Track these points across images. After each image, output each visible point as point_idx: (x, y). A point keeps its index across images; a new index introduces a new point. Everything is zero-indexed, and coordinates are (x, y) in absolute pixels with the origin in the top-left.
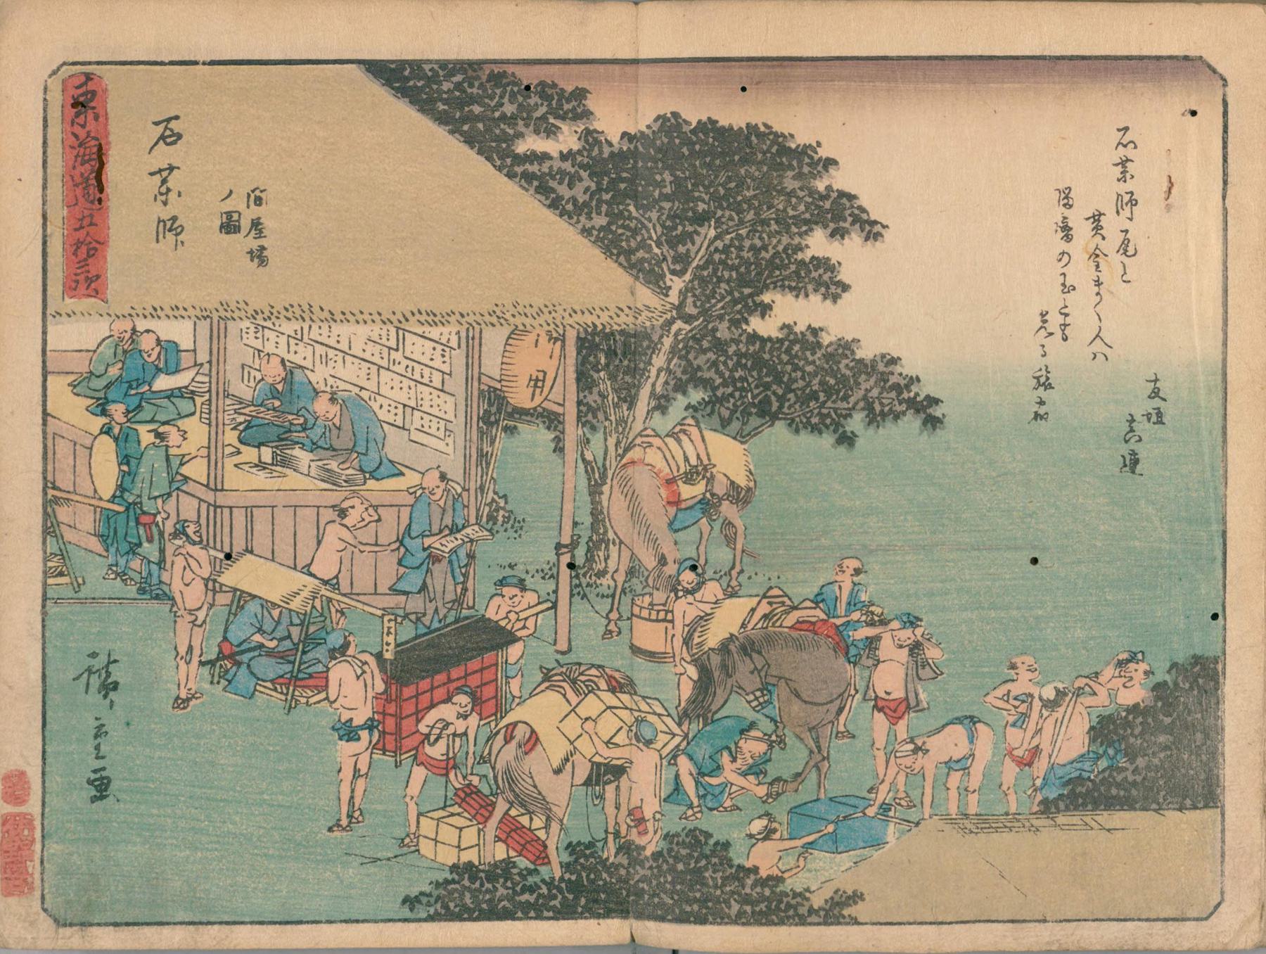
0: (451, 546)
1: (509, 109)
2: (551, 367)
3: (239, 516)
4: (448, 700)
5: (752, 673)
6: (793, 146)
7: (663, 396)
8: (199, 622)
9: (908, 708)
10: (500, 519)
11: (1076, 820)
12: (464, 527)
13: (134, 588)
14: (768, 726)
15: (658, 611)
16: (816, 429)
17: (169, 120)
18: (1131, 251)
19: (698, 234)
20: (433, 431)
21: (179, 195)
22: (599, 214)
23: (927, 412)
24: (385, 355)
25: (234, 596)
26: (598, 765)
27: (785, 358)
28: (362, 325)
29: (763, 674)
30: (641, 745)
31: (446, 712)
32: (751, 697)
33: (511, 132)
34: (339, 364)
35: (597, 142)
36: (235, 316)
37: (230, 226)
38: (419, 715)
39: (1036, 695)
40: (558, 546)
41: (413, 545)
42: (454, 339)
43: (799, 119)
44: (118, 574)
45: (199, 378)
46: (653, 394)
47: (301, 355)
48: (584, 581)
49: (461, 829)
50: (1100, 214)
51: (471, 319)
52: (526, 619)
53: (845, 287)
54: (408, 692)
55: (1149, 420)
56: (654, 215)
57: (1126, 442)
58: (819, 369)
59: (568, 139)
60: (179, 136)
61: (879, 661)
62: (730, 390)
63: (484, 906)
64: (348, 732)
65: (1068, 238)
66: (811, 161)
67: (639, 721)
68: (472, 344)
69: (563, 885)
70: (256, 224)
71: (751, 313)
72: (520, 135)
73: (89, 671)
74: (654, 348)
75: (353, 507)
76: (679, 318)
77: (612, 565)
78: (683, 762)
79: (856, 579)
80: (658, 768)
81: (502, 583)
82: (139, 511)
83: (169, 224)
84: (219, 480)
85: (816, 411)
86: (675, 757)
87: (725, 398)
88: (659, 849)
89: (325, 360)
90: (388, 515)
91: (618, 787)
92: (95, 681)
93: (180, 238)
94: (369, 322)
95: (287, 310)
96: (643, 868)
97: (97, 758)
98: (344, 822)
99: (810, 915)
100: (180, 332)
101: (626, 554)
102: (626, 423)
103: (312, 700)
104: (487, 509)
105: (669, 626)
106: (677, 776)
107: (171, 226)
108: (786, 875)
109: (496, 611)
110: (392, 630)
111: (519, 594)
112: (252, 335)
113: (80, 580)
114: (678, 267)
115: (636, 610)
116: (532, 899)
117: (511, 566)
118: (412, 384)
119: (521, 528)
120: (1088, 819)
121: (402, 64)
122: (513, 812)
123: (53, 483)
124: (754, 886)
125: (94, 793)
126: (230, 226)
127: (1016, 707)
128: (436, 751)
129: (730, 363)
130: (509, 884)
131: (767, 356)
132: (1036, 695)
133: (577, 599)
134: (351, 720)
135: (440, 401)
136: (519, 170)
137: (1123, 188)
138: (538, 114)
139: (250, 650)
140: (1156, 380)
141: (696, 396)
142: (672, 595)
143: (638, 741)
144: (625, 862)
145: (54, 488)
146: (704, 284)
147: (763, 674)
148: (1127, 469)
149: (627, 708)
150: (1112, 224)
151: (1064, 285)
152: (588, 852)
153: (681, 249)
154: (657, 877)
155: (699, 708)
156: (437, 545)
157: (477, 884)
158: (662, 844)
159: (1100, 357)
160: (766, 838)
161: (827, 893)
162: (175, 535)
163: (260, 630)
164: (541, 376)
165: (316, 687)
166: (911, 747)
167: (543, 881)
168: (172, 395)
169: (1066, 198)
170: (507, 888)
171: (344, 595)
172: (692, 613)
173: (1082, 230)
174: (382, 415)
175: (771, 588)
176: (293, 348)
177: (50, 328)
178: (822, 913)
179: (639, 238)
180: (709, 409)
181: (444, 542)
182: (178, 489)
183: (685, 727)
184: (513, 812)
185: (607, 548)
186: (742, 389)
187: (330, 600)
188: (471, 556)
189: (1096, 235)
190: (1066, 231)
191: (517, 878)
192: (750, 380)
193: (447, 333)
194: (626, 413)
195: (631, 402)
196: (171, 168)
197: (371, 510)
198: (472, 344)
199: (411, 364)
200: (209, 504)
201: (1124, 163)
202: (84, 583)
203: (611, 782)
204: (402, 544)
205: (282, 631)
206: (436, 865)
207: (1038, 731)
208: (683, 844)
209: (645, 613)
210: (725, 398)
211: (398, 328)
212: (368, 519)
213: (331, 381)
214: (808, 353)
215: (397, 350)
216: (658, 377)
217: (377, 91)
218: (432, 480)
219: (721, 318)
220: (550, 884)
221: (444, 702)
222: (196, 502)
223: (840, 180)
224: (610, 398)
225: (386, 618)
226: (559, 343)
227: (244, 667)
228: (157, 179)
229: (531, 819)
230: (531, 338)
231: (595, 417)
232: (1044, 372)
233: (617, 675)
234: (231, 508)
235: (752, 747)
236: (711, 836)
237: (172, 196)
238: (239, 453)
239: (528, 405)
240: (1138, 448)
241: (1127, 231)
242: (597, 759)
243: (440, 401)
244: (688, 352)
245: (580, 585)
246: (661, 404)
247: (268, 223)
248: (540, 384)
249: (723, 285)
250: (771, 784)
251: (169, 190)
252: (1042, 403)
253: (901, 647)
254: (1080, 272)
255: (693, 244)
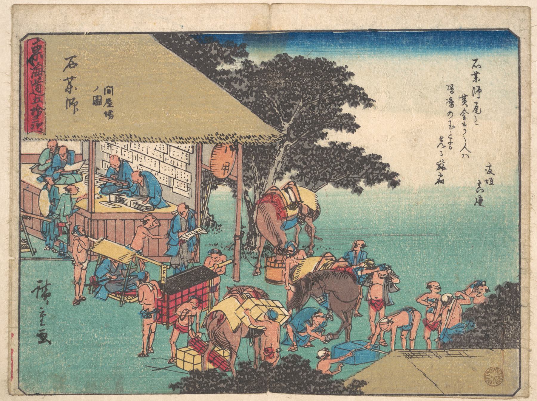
0: (190, 236)
1: (214, 52)
2: (231, 160)
3: (101, 223)
4: (189, 301)
5: (319, 289)
6: (335, 67)
7: (280, 173)
8: (84, 268)
9: (385, 304)
10: (211, 225)
11: (456, 352)
12: (195, 228)
13: (57, 254)
14: (325, 311)
15: (279, 264)
16: (346, 186)
17: (72, 58)
18: (479, 111)
19: (295, 104)
20: (183, 188)
21: (76, 89)
22: (252, 96)
24: (162, 156)
25: (99, 257)
27: (332, 156)
28: (152, 143)
29: (323, 289)
30: (271, 321)
32: (318, 299)
33: (215, 62)
34: (144, 158)
35: (252, 66)
36: (99, 139)
38: (176, 307)
39: (440, 299)
40: (235, 236)
41: (174, 236)
42: (191, 150)
43: (339, 58)
44: (50, 248)
45: (84, 166)
46: (276, 172)
47: (127, 156)
48: (246, 251)
49: (194, 356)
50: (466, 96)
51: (198, 141)
52: (221, 267)
53: (358, 126)
54: (172, 297)
55: (487, 183)
56: (276, 97)
57: (477, 192)
58: (347, 161)
59: (238, 65)
61: (373, 284)
62: (309, 170)
63: (204, 389)
64: (146, 314)
66: (344, 74)
67: (270, 311)
68: (198, 151)
69: (237, 380)
70: (108, 101)
71: (318, 138)
72: (219, 63)
73: (38, 288)
74: (277, 152)
75: (149, 220)
76: (287, 139)
77: (258, 244)
78: (289, 327)
79: (363, 250)
80: (279, 331)
81: (212, 252)
82: (59, 222)
83: (71, 101)
85: (345, 179)
86: (286, 325)
87: (307, 173)
88: (279, 364)
89: (137, 158)
90: (164, 223)
91: (260, 339)
92: (40, 293)
95: (121, 137)
96: (272, 372)
97: (41, 325)
98: (145, 353)
99: (343, 391)
100: (75, 146)
101: (264, 240)
102: (263, 184)
103: (131, 301)
104: (205, 221)
105: (284, 270)
106: (287, 333)
107: (71, 103)
108: (333, 374)
109: (209, 264)
110: (165, 272)
111: (219, 257)
112: (106, 148)
113: (34, 250)
114: (287, 118)
115: (268, 264)
116: (224, 386)
117: (215, 245)
118: (174, 168)
119: (219, 229)
120: (461, 352)
121: (168, 34)
122: (216, 349)
123: (23, 210)
124: (320, 379)
125: (40, 340)
126: (97, 102)
127: (431, 305)
129: (309, 159)
130: (215, 380)
131: (325, 156)
132: (440, 299)
133: (243, 258)
134: (148, 309)
135: (185, 176)
136: (218, 78)
137: (475, 85)
138: (226, 54)
140: (490, 166)
141: (294, 172)
142: (285, 256)
143: (270, 319)
144: (264, 371)
145: (24, 211)
146: (297, 127)
147: (323, 289)
148: (478, 204)
149: (264, 305)
150: (471, 101)
151: (450, 126)
152: (248, 366)
153: (288, 111)
154: (278, 376)
155: (296, 303)
156: (184, 236)
157: (201, 380)
160: (325, 359)
161: (350, 381)
162: (75, 231)
163: (110, 272)
164: (227, 165)
165: (133, 295)
166: (386, 320)
167: (229, 378)
168: (73, 173)
169: (451, 89)
170: (213, 381)
171: (146, 257)
174: (161, 181)
175: (327, 253)
176: (123, 153)
177: (22, 144)
178: (349, 390)
179: (269, 106)
180: (300, 178)
181: (187, 234)
182: (76, 212)
183: (291, 311)
184: (216, 349)
185: (255, 238)
186: (314, 170)
187: (140, 259)
188: (198, 241)
190: (451, 102)
191: (218, 377)
192: (318, 166)
193: (187, 146)
194: (263, 180)
195: (266, 175)
196: (72, 78)
197: (156, 221)
198: (198, 151)
199: (173, 160)
200: (89, 219)
202: (36, 251)
203: (257, 336)
205: (119, 272)
206: (184, 371)
207: (441, 315)
208: (289, 362)
210: (307, 173)
211: (167, 145)
212: (155, 225)
213: (140, 167)
214: (342, 154)
215: (167, 154)
216: (278, 165)
218: (182, 208)
219: (305, 140)
220: (232, 379)
221: (187, 302)
222: (83, 217)
223: (355, 81)
224: (257, 174)
225: (163, 267)
226: (235, 151)
227: (103, 287)
229: (224, 352)
230: (223, 149)
231: (250, 182)
232: (442, 162)
233: (259, 291)
234: (98, 220)
235: (318, 320)
236: (302, 358)
238: (101, 197)
239: (222, 176)
240: (483, 195)
241: (477, 103)
242: (251, 326)
245: (244, 253)
247: (113, 99)
249: (306, 126)
250: (327, 336)
252: (441, 176)
253: (382, 278)
254: (457, 120)
255: (293, 109)
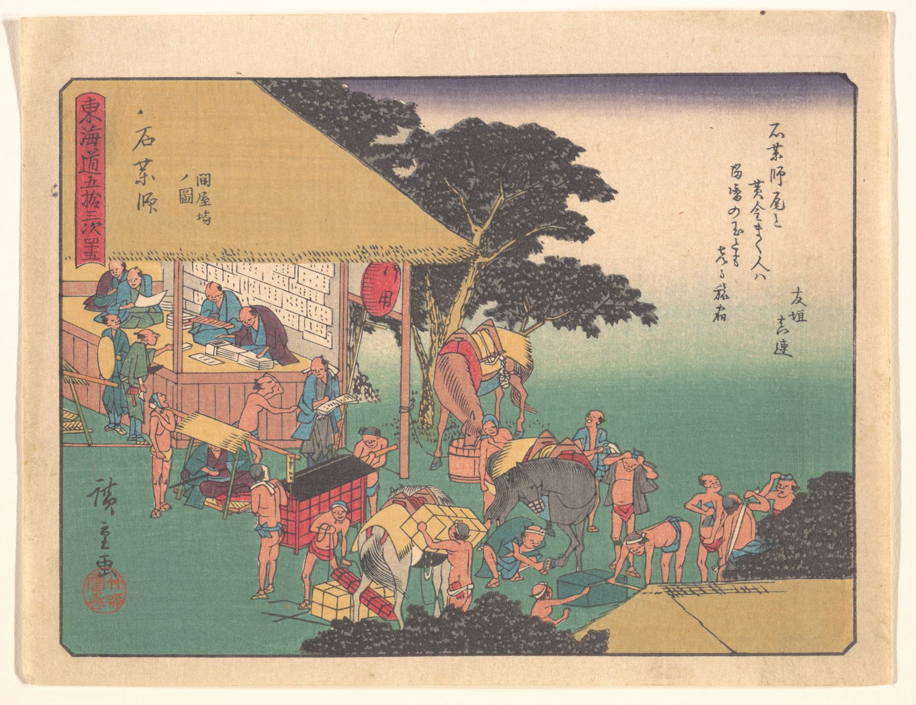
18: (780, 206)
23: (647, 314)
26: (429, 553)
31: (327, 517)
37: (185, 198)
53: (591, 232)
55: (794, 319)
59: (402, 136)
60: (153, 139)
65: (737, 198)
73: (97, 490)
84: (180, 365)
92: (101, 498)
93: (153, 206)
94: (276, 260)
100: (154, 269)
107: (146, 201)
109: (360, 451)
126: (185, 198)
128: (323, 545)
137: (775, 165)
139: (202, 477)
141: (492, 305)
150: (768, 189)
151: (735, 230)
158: (475, 605)
159: (761, 277)
169: (736, 170)
172: (492, 450)
173: (747, 192)
189: (755, 195)
190: (736, 193)
196: (147, 161)
201: (776, 147)
204: (298, 407)
209: (460, 452)
217: (277, 108)
228: (138, 167)
237: (149, 179)
242: (428, 549)
243: (323, 313)
244: (487, 278)
246: (469, 311)
248: (388, 300)
251: (145, 175)
254: (747, 221)
